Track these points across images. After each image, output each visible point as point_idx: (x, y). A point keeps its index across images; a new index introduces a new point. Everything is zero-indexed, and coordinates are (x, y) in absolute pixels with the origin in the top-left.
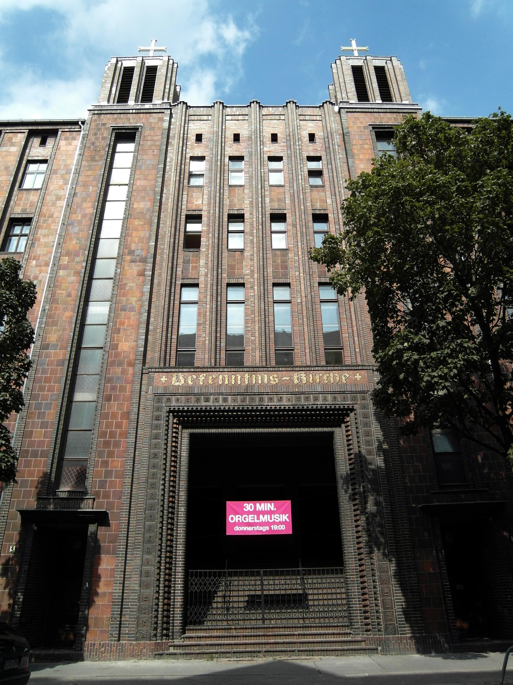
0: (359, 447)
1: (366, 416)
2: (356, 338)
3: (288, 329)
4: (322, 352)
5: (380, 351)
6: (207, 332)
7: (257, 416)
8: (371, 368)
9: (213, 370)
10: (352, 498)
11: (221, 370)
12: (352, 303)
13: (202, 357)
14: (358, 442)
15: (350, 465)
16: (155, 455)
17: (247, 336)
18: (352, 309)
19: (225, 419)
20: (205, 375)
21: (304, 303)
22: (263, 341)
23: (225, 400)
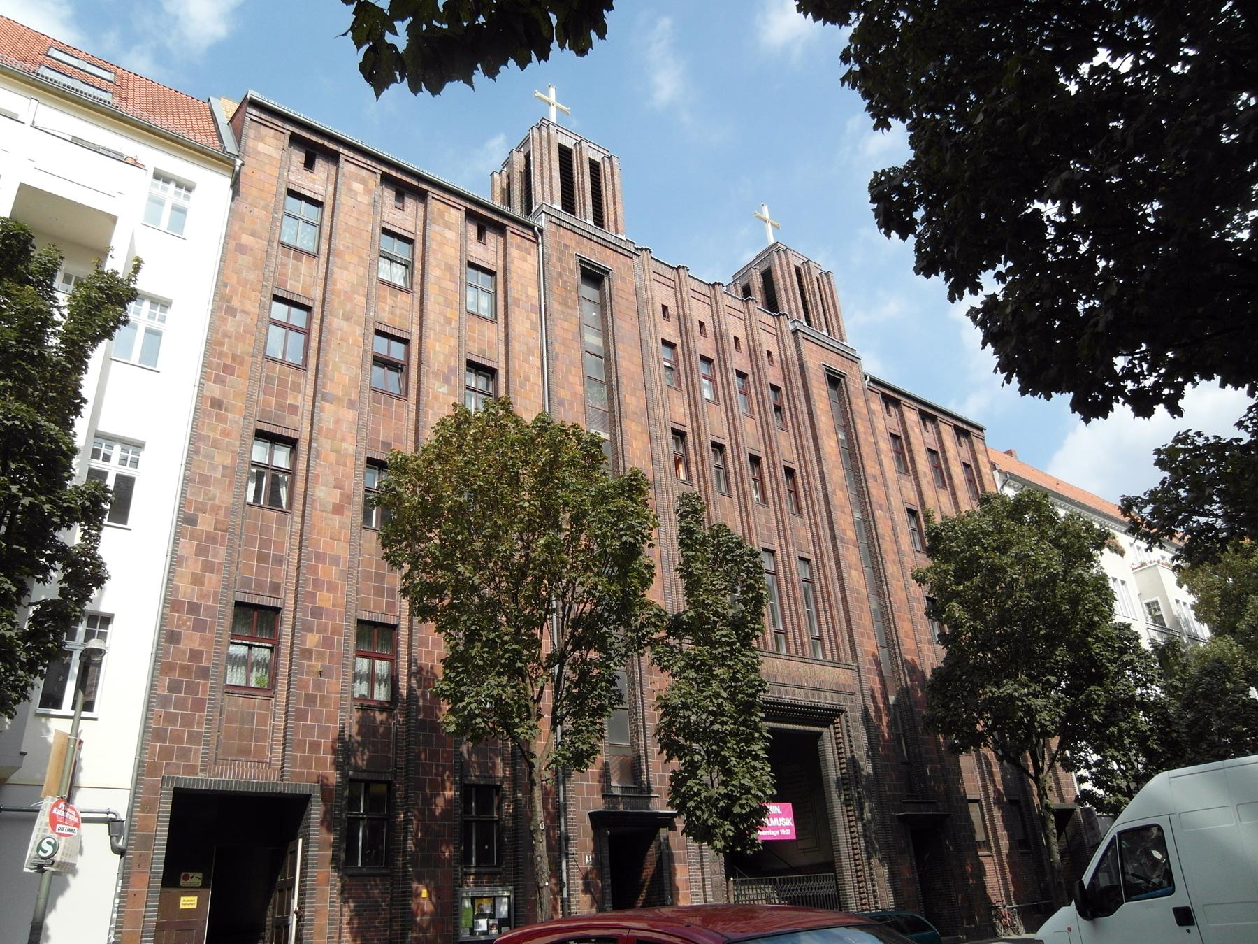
10: (847, 803)
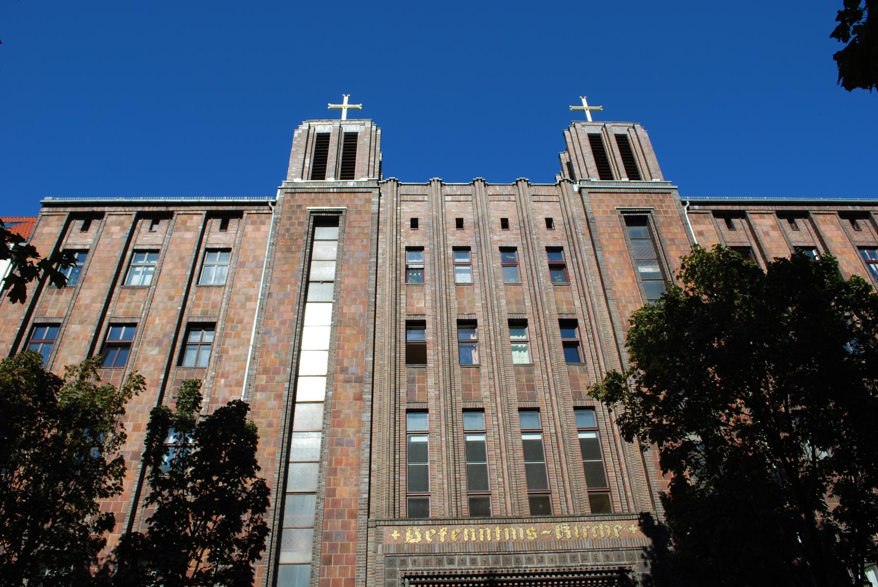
6: (445, 472)
20: (446, 529)
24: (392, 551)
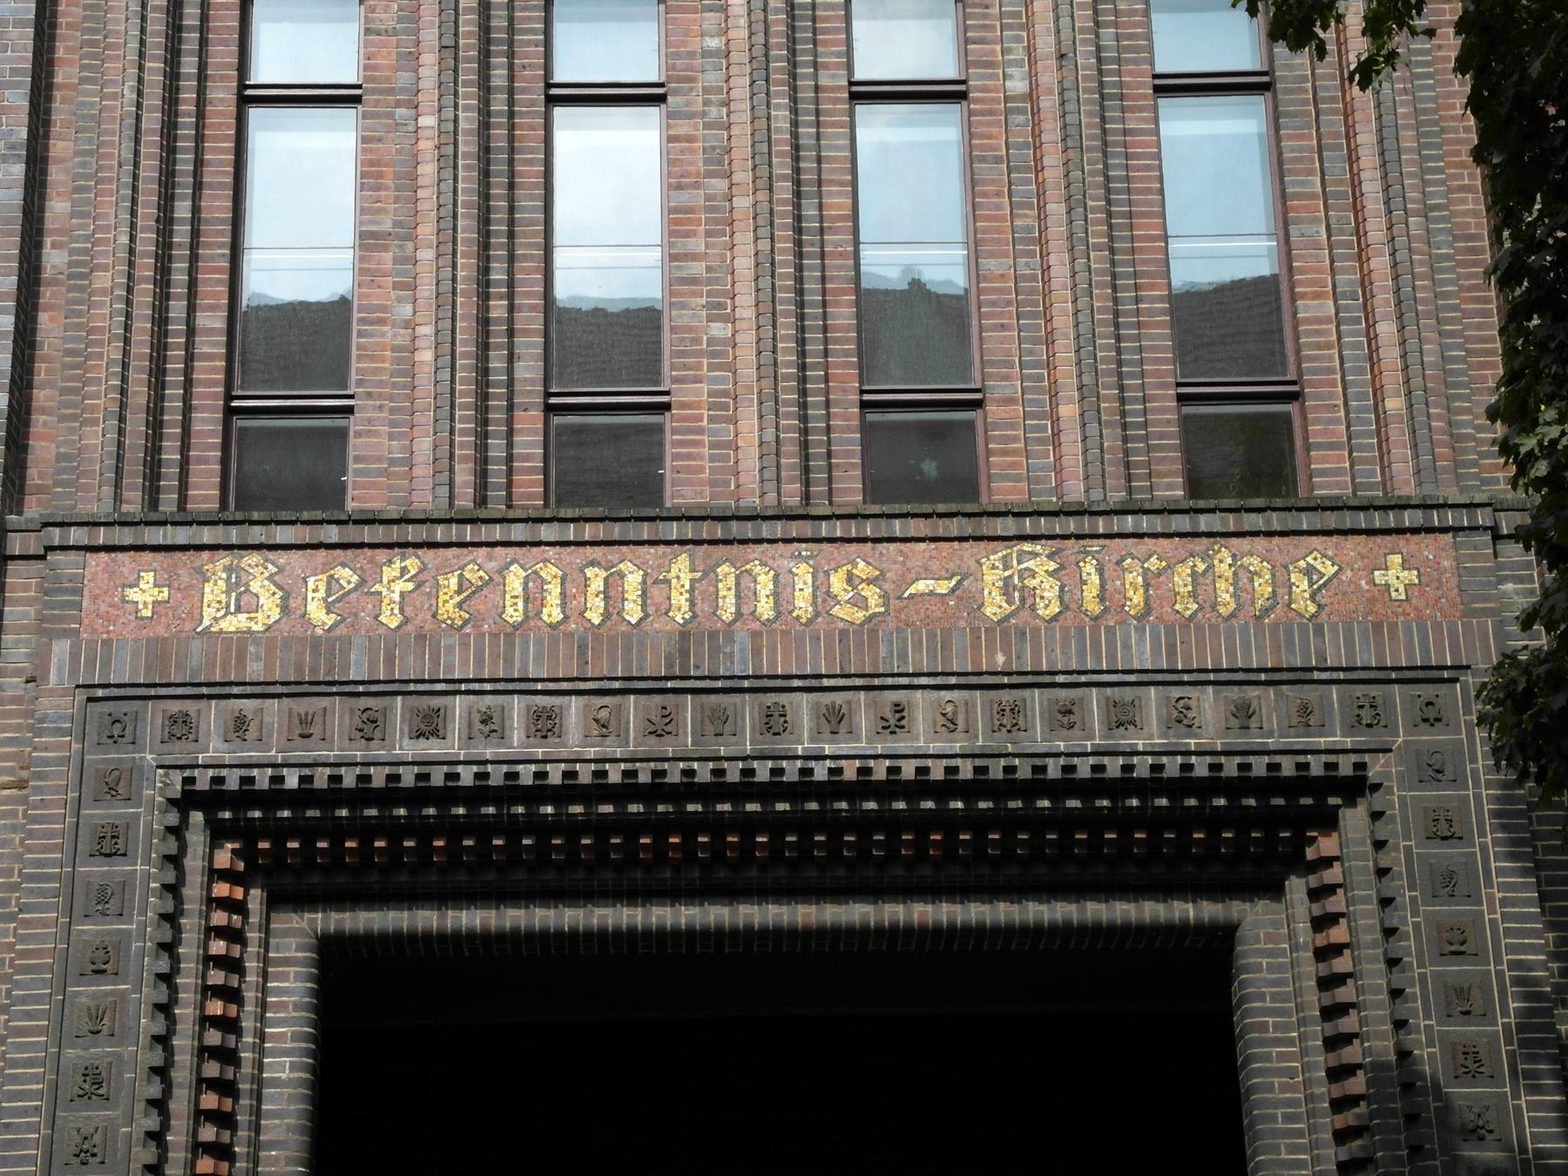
0: (1400, 1024)
1: (1443, 828)
2: (1386, 329)
3: (945, 269)
4: (1165, 415)
5: (1548, 413)
6: (426, 289)
7: (748, 826)
8: (1482, 517)
9: (469, 533)
11: (518, 532)
12: (1362, 99)
13: (396, 449)
14: (1396, 994)
15: (1341, 1136)
16: (94, 1083)
17: (683, 318)
18: (1366, 138)
19: (543, 848)
20: (413, 564)
21: (1049, 103)
22: (786, 346)
23: (545, 725)
24: (122, 672)
